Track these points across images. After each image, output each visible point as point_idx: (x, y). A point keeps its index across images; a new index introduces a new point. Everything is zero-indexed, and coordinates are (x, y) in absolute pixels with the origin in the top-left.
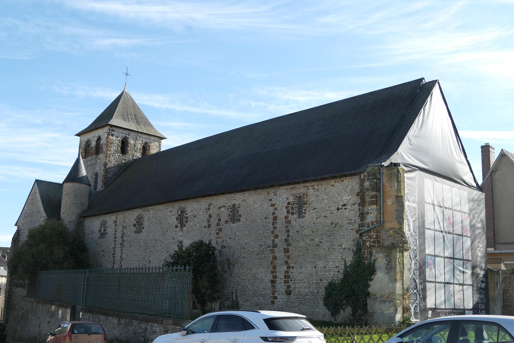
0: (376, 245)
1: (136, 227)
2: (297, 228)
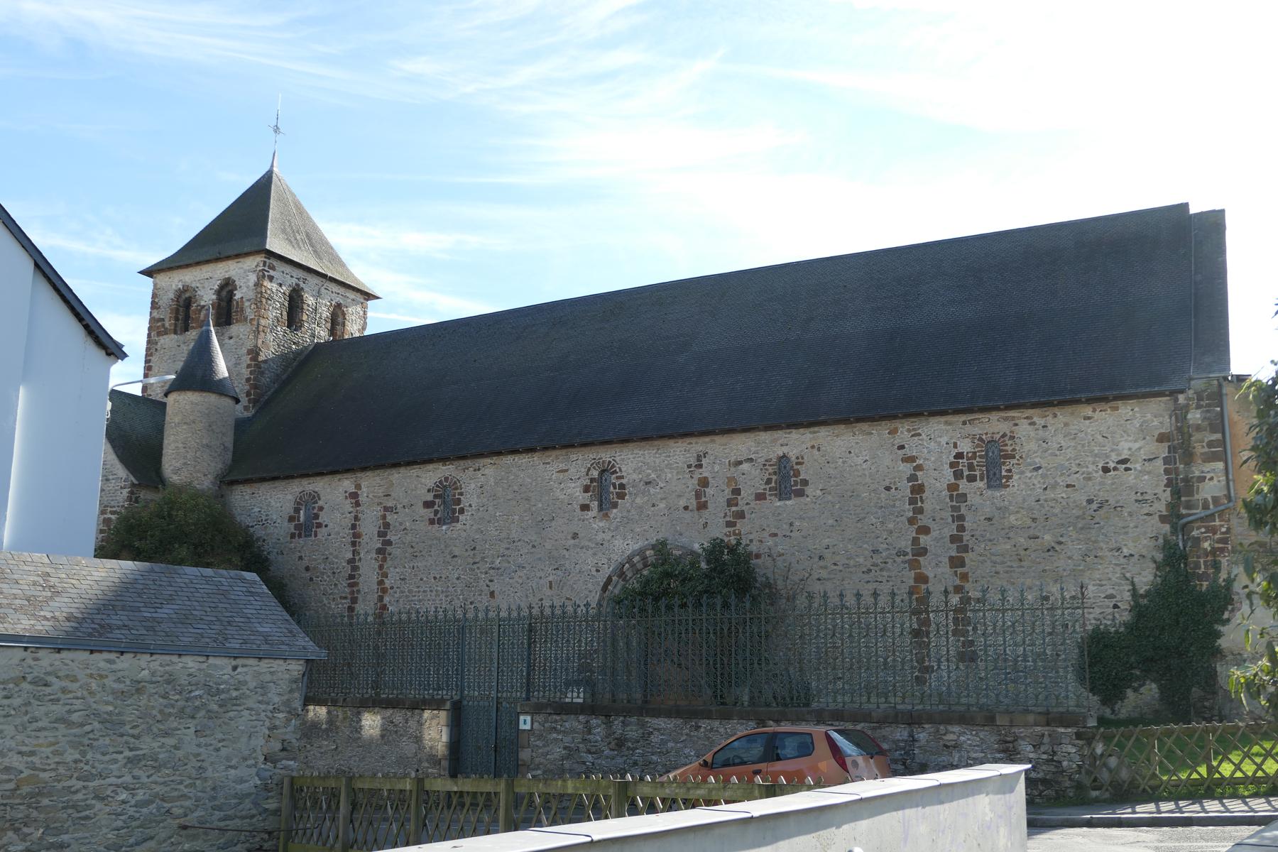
0: (1230, 548)
1: (433, 510)
2: (988, 510)
